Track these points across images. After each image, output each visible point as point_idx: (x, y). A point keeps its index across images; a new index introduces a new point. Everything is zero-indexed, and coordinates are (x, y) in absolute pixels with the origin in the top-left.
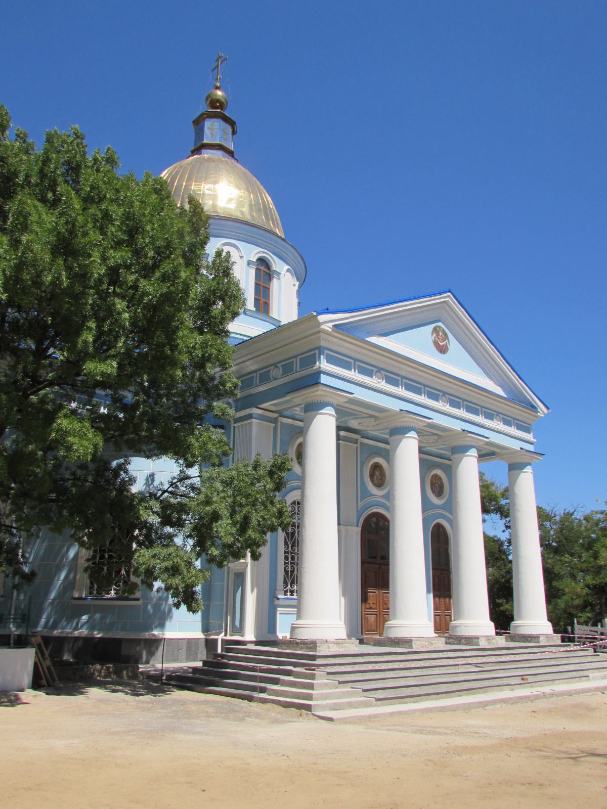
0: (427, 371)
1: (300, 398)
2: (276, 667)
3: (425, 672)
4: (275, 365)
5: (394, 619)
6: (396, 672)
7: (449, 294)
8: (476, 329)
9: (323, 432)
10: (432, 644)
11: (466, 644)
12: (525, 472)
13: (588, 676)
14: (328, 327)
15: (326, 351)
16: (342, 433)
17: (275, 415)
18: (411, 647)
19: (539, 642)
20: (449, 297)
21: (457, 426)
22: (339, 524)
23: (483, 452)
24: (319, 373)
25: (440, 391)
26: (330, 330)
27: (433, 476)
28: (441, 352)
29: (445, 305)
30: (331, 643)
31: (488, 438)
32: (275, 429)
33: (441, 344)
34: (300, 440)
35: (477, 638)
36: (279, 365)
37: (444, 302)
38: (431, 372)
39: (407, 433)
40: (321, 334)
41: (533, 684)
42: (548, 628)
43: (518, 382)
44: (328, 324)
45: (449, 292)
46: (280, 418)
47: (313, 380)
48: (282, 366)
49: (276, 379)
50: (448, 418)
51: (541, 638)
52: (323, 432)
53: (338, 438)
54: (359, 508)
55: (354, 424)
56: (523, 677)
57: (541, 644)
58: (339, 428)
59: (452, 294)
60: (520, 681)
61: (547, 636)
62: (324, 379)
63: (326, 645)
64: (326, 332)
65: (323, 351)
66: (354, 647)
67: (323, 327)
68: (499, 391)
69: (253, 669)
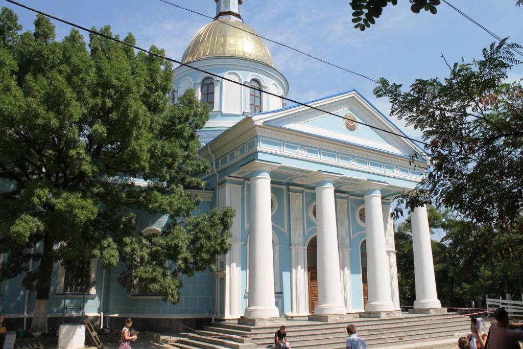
0: (311, 137)
1: (246, 170)
2: (482, 312)
3: (327, 336)
4: (236, 149)
5: (424, 298)
6: (305, 337)
7: (354, 92)
8: (376, 113)
9: (263, 187)
10: (343, 318)
11: (373, 317)
12: (376, 196)
13: (453, 335)
14: (260, 123)
15: (261, 138)
16: (338, 194)
17: (242, 180)
18: (327, 321)
19: (429, 314)
20: (354, 94)
21: (364, 177)
22: (339, 247)
23: (393, 192)
24: (257, 152)
25: (350, 156)
26: (261, 125)
27: (361, 210)
28: (351, 130)
29: (352, 99)
30: (265, 320)
31: (341, 174)
32: (348, 202)
33: (351, 125)
34: (361, 207)
35: (379, 313)
36: (238, 149)
37: (352, 97)
38: (318, 139)
39: (258, 175)
40: (256, 128)
41: (406, 342)
42: (437, 304)
43: (412, 145)
44: (259, 121)
45: (354, 90)
46: (246, 181)
47: (253, 156)
48: (240, 149)
49: (237, 157)
50: (355, 171)
51: (431, 311)
52: (263, 187)
53: (335, 197)
54: (305, 234)
55: (343, 189)
56: (400, 338)
57: (431, 315)
58: (336, 191)
59: (356, 91)
60: (398, 340)
61: (436, 309)
62: (260, 156)
63: (262, 322)
64: (259, 126)
65: (259, 138)
66: (400, 315)
67: (256, 123)
68: (397, 151)
69: (231, 339)
